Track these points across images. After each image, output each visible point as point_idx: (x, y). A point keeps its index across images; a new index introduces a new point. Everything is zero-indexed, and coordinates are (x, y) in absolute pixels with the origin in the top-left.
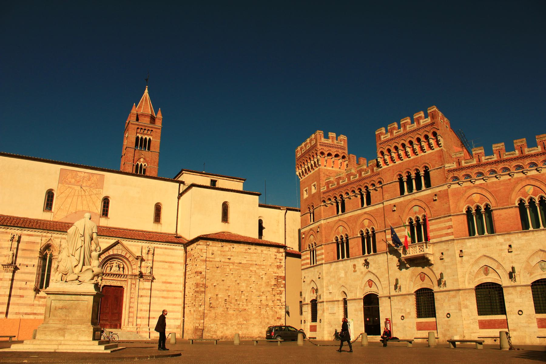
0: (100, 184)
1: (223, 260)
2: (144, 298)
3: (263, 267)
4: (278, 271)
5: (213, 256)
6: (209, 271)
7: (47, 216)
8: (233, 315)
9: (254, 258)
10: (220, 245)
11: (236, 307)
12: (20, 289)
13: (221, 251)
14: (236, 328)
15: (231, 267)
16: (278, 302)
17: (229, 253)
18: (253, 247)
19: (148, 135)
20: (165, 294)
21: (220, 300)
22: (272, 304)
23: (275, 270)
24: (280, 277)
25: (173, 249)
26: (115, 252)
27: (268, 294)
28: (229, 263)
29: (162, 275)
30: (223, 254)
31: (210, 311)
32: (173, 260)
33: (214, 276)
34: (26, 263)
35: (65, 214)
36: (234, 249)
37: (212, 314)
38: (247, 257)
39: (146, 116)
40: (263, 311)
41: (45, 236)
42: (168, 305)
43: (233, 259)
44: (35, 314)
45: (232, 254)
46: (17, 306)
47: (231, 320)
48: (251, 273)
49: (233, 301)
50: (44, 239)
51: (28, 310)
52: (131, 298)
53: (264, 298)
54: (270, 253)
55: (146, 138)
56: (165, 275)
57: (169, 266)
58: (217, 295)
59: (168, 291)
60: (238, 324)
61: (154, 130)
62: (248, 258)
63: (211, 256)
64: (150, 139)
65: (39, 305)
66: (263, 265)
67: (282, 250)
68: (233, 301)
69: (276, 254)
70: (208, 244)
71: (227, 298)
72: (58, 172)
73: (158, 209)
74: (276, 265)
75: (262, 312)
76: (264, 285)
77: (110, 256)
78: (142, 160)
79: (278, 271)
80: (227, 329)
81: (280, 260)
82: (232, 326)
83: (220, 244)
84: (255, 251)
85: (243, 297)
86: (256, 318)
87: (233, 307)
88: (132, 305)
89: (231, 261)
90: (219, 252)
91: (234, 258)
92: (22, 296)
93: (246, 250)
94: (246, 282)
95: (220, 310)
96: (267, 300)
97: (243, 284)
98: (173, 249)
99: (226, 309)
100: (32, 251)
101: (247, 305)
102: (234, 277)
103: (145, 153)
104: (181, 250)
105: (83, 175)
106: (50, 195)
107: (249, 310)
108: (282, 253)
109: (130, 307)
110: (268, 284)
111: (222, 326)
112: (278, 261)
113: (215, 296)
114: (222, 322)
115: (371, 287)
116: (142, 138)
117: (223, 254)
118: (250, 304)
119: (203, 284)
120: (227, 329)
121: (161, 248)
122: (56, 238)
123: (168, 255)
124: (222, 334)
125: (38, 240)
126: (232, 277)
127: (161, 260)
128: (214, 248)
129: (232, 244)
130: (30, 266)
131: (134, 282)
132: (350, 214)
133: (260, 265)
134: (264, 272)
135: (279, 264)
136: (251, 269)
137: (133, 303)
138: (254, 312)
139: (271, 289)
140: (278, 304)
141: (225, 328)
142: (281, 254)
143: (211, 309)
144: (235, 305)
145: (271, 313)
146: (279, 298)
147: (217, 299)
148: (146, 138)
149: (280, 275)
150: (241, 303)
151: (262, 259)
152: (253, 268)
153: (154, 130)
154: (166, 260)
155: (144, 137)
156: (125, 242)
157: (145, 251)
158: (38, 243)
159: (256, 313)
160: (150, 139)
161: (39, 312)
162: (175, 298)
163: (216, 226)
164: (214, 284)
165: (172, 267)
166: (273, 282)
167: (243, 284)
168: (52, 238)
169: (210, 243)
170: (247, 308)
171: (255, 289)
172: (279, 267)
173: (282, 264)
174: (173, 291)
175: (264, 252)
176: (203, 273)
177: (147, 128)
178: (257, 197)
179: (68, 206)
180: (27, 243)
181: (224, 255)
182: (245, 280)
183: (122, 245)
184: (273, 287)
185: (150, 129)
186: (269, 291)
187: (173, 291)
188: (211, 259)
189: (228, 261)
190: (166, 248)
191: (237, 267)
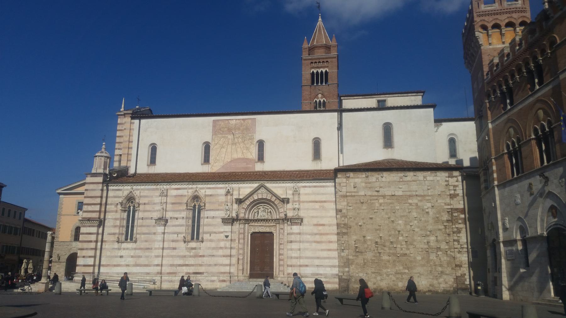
0: (249, 130)
1: (369, 193)
2: (293, 244)
3: (427, 198)
4: (452, 202)
5: (355, 190)
6: (351, 208)
7: (206, 169)
8: (389, 261)
9: (414, 187)
10: (364, 176)
11: (391, 252)
12: (173, 241)
13: (366, 183)
14: (394, 278)
15: (381, 201)
16: (456, 243)
17: (377, 184)
18: (411, 174)
19: (324, 67)
20: (318, 238)
21: (369, 243)
22: (447, 247)
23: (448, 200)
24: (457, 209)
25: (323, 187)
26: (260, 197)
27: (438, 234)
28: (378, 196)
29: (313, 217)
30: (369, 185)
31: (357, 256)
32: (324, 199)
33: (358, 214)
34: (176, 216)
35: (222, 164)
36: (384, 179)
37: (360, 260)
38: (404, 186)
39: (320, 47)
40: (433, 257)
41: (192, 188)
42: (322, 250)
43: (384, 191)
44: (187, 265)
45: (382, 185)
46: (171, 258)
47: (387, 267)
48: (411, 207)
49: (388, 244)
50: (190, 191)
51: (181, 262)
52: (281, 244)
53: (432, 238)
54: (438, 178)
55: (322, 72)
56: (316, 217)
57: (320, 207)
58: (364, 237)
59: (321, 234)
60: (397, 273)
61: (329, 60)
62: (405, 187)
63: (353, 190)
64: (326, 71)
65: (190, 257)
66: (429, 196)
67: (456, 173)
68: (388, 244)
69: (447, 179)
70: (348, 175)
71: (378, 240)
72: (211, 124)
73: (317, 144)
74: (448, 193)
75: (431, 258)
76: (431, 221)
77: (255, 201)
78: (320, 96)
79: (452, 202)
80: (382, 280)
81: (454, 186)
82: (388, 275)
83: (363, 175)
84: (414, 178)
85: (401, 238)
86: (423, 266)
87: (388, 251)
88: (281, 252)
89: (380, 194)
90: (363, 184)
91: (385, 190)
92: (174, 249)
93: (401, 178)
94: (404, 219)
95: (369, 256)
96: (437, 241)
97: (400, 222)
98: (323, 187)
99: (378, 255)
100: (180, 203)
101: (408, 249)
102: (387, 214)
103: (324, 87)
104: (332, 186)
105: (233, 122)
106: (207, 147)
107: (412, 255)
108: (456, 177)
109: (280, 254)
110: (437, 220)
111: (374, 275)
112: (452, 188)
113: (362, 239)
114: (373, 270)
115: (196, 198)
116: (317, 72)
117: (369, 185)
118: (412, 247)
119: (344, 224)
120: (382, 280)
121: (310, 187)
122: (201, 188)
123: (318, 194)
124: (375, 286)
125: (184, 192)
126: (383, 213)
127: (310, 200)
128: (356, 180)
129: (380, 173)
130: (180, 218)
131: (282, 226)
132: (520, 107)
133: (424, 196)
134: (429, 205)
135: (452, 192)
136: (410, 201)
137: (283, 249)
138: (419, 258)
139: (443, 227)
140: (456, 246)
141: (379, 278)
142: (455, 179)
143: (358, 254)
144: (390, 249)
145: (445, 258)
146: (456, 238)
147: (365, 242)
148: (322, 72)
149: (455, 207)
150: (399, 246)
151: (426, 187)
152: (414, 201)
153: (329, 60)
154: (317, 200)
155: (320, 71)
156: (269, 185)
157: (290, 192)
158: (185, 196)
159: (423, 258)
160: (326, 71)
161: (190, 263)
162: (330, 242)
163: (377, 153)
164: (360, 224)
165: (323, 207)
166: (445, 217)
167: (400, 222)
168: (197, 189)
169: (351, 174)
170: (408, 252)
171: (418, 227)
172: (452, 196)
173: (457, 192)
174: (327, 234)
175: (428, 178)
176: (344, 211)
177: (321, 61)
178: (432, 110)
179: (223, 155)
180: (176, 196)
181: (370, 188)
182: (401, 216)
183: (266, 188)
184: (445, 224)
185: (325, 60)
186: (440, 230)
187: (327, 234)
188: (353, 194)
189: (376, 194)
190: (315, 187)
191: (389, 201)
